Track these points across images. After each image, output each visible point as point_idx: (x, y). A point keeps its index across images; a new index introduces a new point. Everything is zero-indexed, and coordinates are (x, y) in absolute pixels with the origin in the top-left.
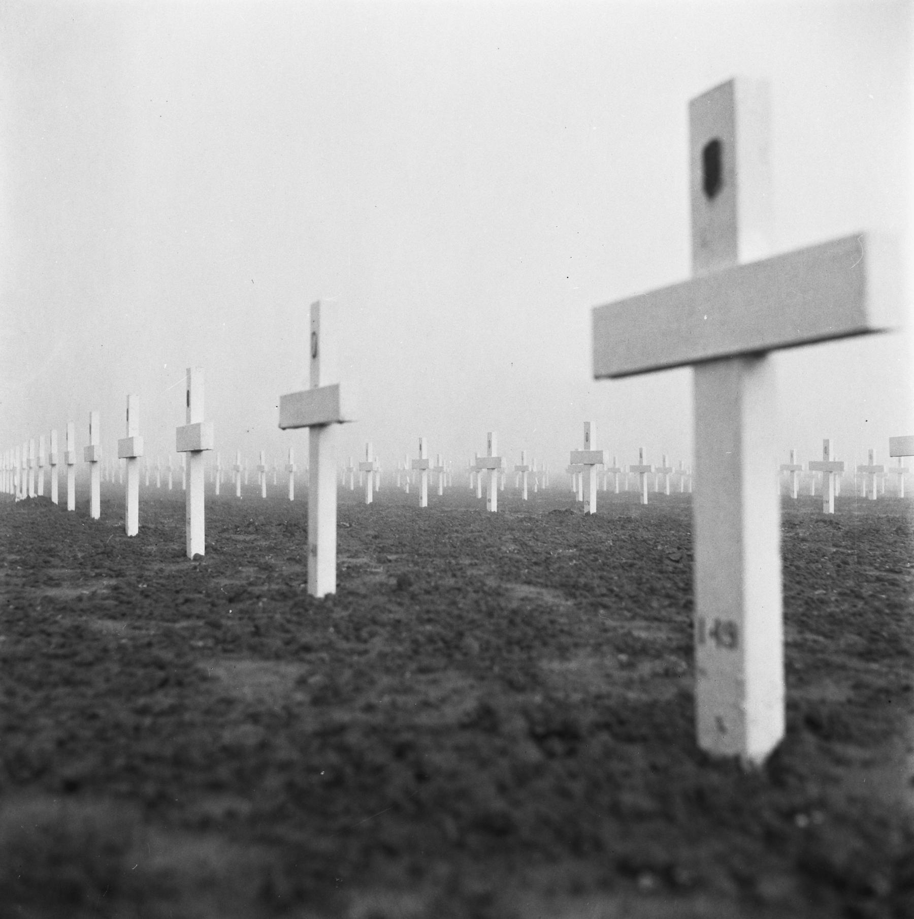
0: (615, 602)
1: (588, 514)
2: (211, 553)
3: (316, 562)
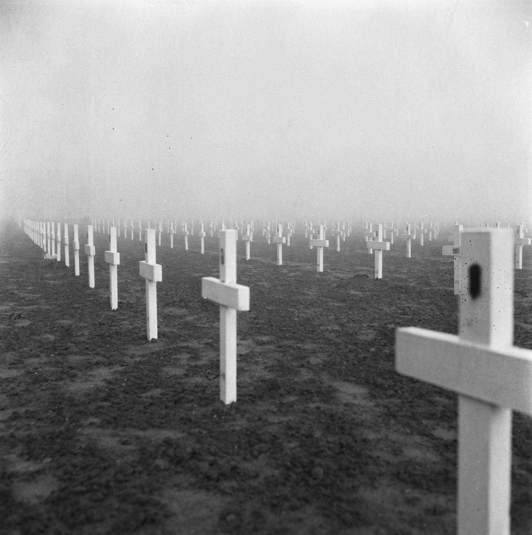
0: (384, 308)
1: (377, 279)
2: (162, 337)
3: (225, 383)
